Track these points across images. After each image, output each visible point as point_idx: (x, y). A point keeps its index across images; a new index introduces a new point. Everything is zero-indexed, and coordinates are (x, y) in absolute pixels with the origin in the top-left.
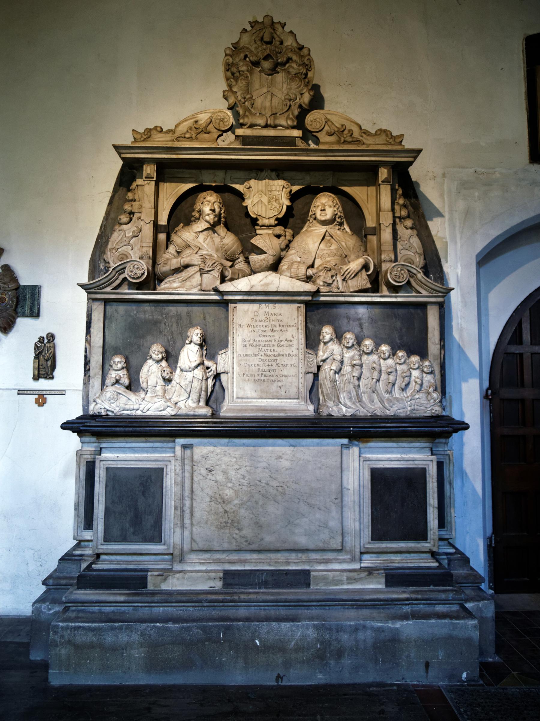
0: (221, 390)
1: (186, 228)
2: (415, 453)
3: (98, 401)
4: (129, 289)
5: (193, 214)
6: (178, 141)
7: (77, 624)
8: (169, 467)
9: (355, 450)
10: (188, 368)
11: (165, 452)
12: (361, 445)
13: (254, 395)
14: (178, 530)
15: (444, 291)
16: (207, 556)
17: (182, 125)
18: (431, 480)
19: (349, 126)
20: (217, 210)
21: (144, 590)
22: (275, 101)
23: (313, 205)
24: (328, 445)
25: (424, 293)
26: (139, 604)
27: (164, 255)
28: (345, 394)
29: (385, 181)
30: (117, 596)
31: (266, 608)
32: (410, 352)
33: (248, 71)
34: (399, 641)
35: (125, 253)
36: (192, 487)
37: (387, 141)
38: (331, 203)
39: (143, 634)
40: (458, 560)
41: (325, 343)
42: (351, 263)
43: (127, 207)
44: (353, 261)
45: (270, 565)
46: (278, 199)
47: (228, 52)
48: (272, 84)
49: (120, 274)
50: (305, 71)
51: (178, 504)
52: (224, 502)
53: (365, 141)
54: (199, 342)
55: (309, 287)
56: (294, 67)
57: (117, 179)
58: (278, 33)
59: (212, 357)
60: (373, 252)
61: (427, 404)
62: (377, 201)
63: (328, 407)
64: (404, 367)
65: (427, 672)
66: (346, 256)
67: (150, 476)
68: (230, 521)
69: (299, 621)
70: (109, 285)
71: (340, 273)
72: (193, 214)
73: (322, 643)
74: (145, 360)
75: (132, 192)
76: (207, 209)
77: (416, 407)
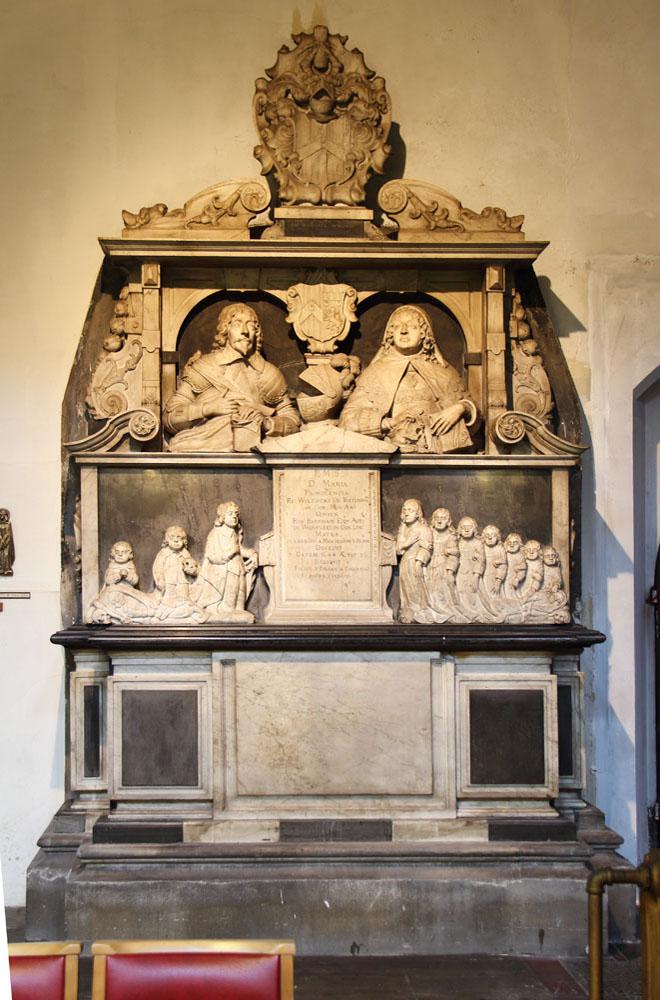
0: (265, 590)
1: (206, 357)
2: (528, 671)
3: (97, 604)
4: (132, 449)
5: (217, 338)
6: (191, 228)
7: (99, 883)
8: (204, 689)
9: (449, 667)
10: (220, 560)
11: (198, 670)
12: (457, 661)
13: (311, 595)
14: (219, 769)
15: (575, 451)
16: (257, 802)
17: (195, 204)
18: (549, 706)
19: (443, 203)
20: (252, 333)
21: (180, 844)
22: (333, 162)
23: (389, 324)
24: (413, 660)
25: (548, 453)
26: (176, 860)
27: (175, 398)
28: (435, 593)
29: (495, 288)
30: (150, 849)
31: (336, 864)
32: (526, 537)
33: (291, 116)
34: (506, 904)
35: (117, 394)
36: (236, 715)
37: (500, 227)
38: (416, 323)
39: (182, 894)
40: (590, 816)
41: (408, 524)
42: (445, 411)
43: (117, 326)
44: (447, 407)
45: (339, 813)
46: (338, 313)
47: (261, 86)
48: (328, 137)
49: (119, 429)
50: (377, 116)
51: (219, 736)
52: (277, 733)
53: (466, 226)
54: (234, 524)
55: (386, 446)
56: (361, 109)
57: (98, 280)
58: (336, 54)
59: (250, 543)
60: (478, 391)
61: (549, 607)
62: (481, 315)
63: (413, 612)
64: (518, 557)
65: (541, 942)
66: (438, 400)
67: (181, 701)
68: (286, 758)
69: (379, 878)
70: (105, 444)
71: (429, 425)
72: (217, 338)
73: (408, 905)
74: (158, 549)
75: (123, 303)
76: (236, 332)
77: (534, 612)
